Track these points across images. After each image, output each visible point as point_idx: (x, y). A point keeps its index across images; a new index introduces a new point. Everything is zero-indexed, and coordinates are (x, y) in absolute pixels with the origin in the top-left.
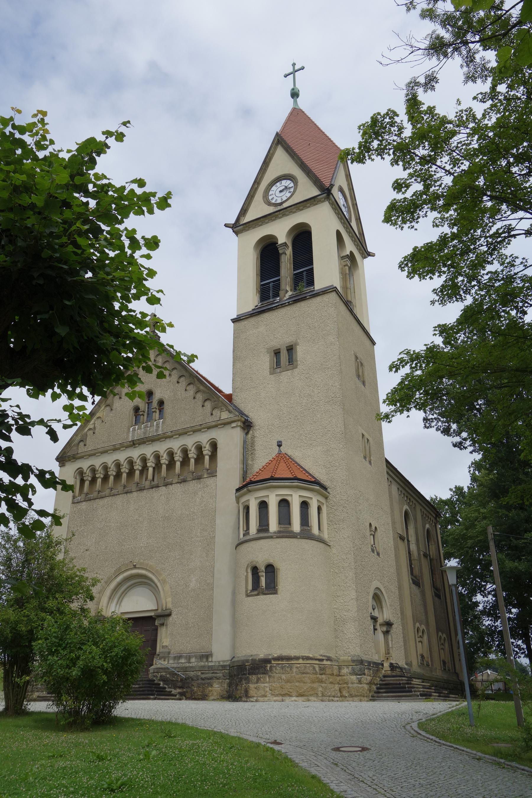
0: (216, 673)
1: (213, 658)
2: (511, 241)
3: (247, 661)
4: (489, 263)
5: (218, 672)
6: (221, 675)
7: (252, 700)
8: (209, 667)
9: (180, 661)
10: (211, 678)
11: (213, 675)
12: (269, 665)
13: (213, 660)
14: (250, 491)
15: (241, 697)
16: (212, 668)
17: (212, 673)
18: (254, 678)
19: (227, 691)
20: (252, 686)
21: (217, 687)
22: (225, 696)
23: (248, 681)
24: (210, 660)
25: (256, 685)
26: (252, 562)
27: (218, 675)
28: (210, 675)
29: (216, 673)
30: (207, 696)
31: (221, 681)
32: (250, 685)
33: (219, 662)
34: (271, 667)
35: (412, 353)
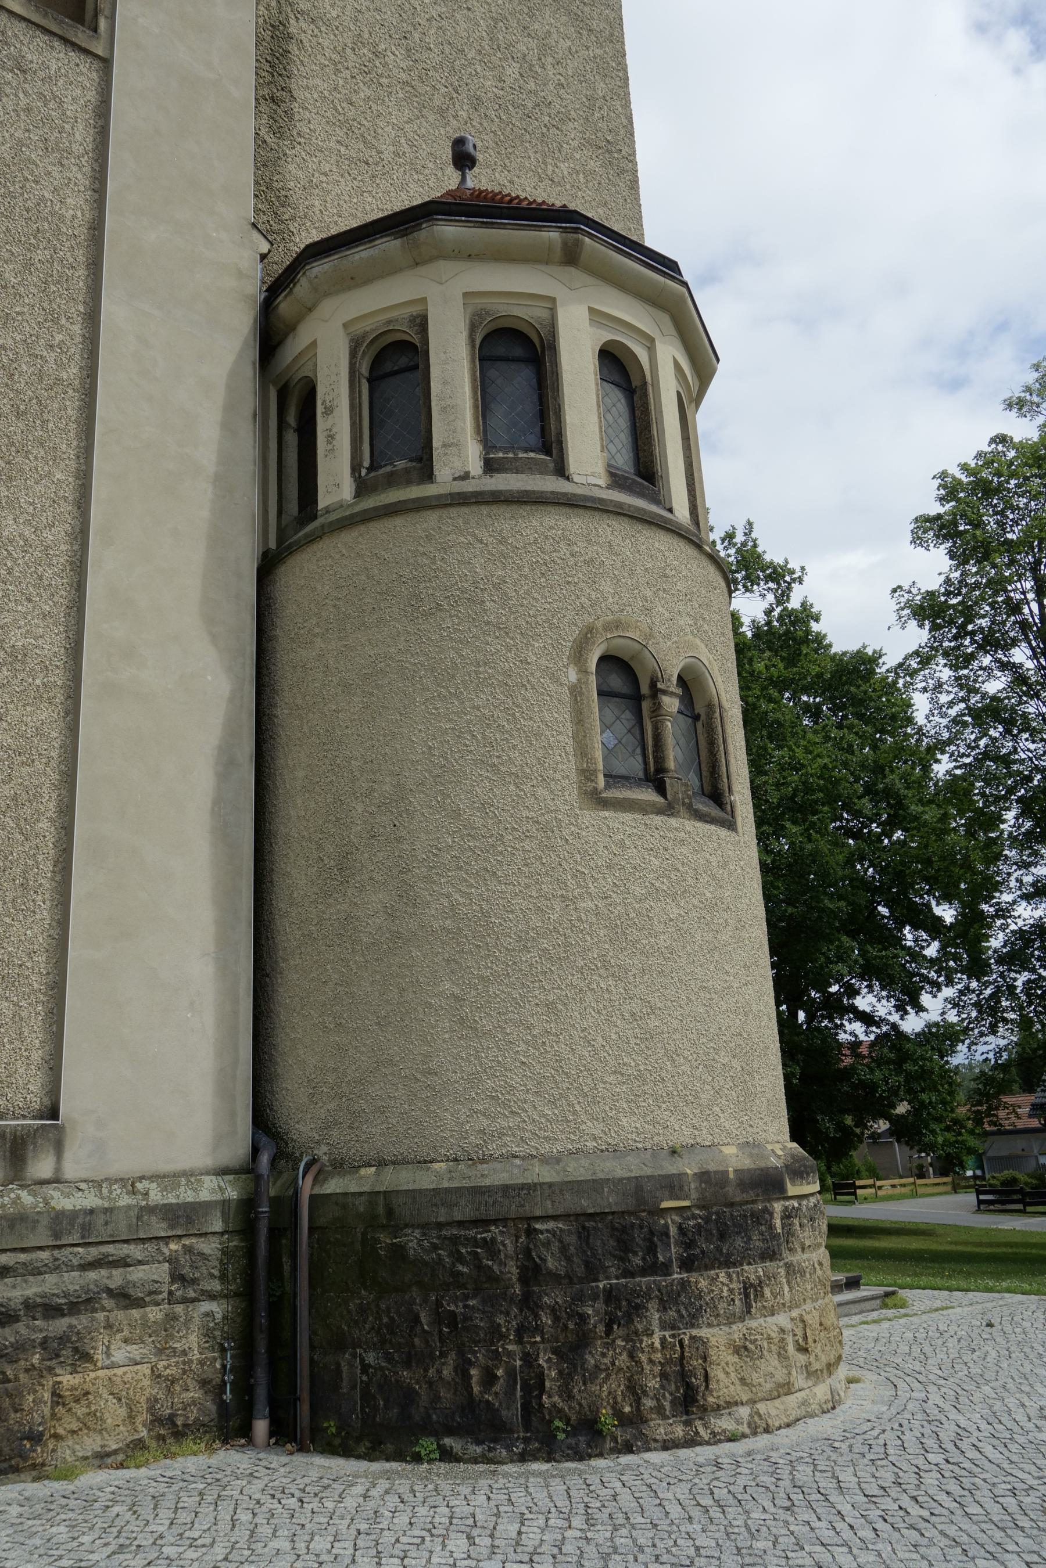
0: (124, 1263)
1: (68, 1155)
2: (942, 500)
3: (673, 1185)
4: (755, 546)
5: (135, 1251)
6: (160, 1272)
7: (724, 1423)
8: (60, 1222)
9: (444, 1232)
10: (75, 1306)
11: (92, 1275)
12: (778, 1207)
13: (70, 1171)
14: (571, 257)
15: (635, 1420)
16: (86, 1229)
17: (85, 1267)
18: (718, 1284)
19: (204, 1383)
20: (716, 1336)
21: (129, 1365)
22: (193, 1414)
23: (685, 1308)
24: (42, 1167)
25: (737, 1330)
26: (618, 625)
27: (137, 1274)
28: (73, 1282)
29: (124, 1263)
30: (36, 1438)
31: (155, 1314)
32: (703, 1332)
33: (130, 1184)
34: (788, 1215)
35: (942, 492)
